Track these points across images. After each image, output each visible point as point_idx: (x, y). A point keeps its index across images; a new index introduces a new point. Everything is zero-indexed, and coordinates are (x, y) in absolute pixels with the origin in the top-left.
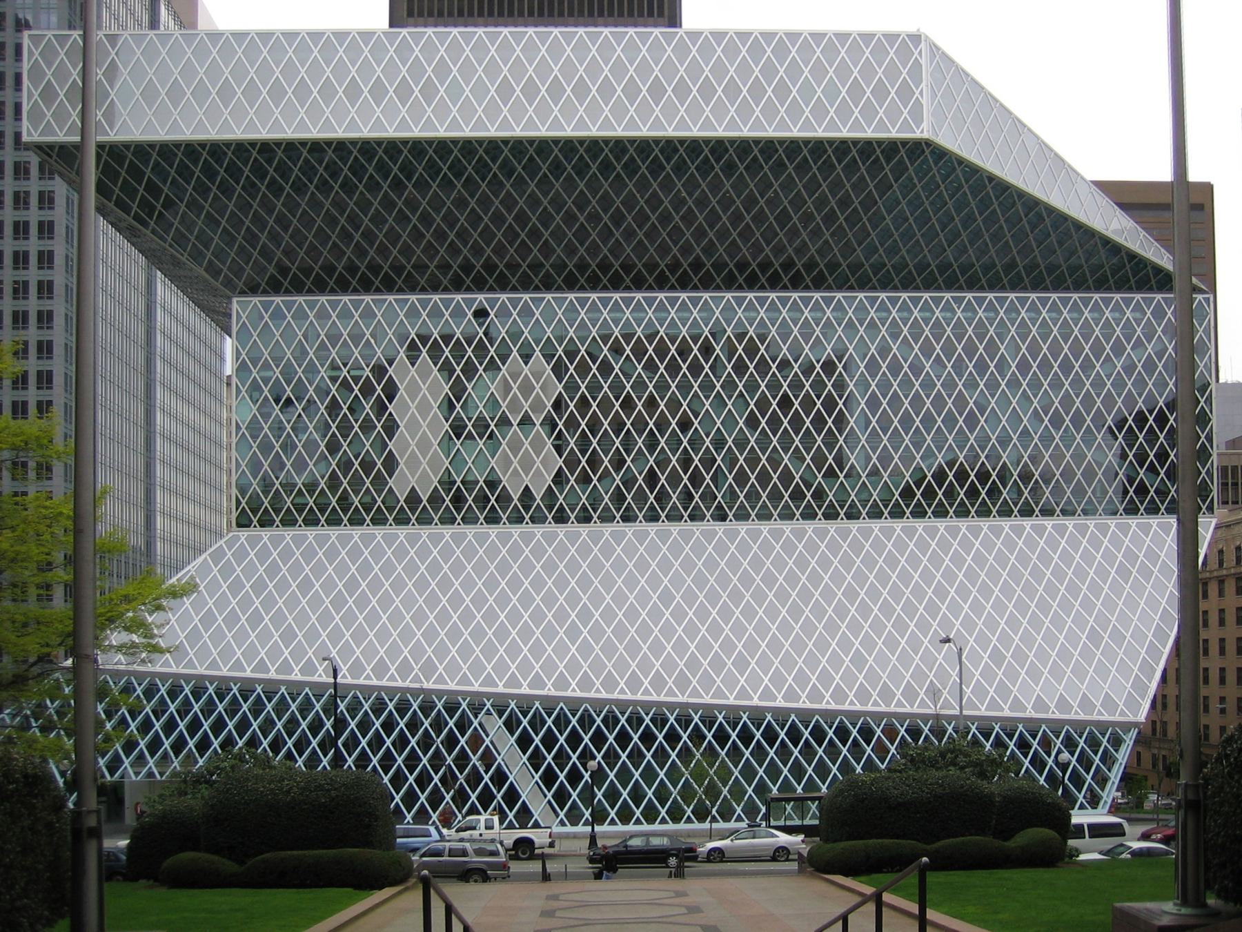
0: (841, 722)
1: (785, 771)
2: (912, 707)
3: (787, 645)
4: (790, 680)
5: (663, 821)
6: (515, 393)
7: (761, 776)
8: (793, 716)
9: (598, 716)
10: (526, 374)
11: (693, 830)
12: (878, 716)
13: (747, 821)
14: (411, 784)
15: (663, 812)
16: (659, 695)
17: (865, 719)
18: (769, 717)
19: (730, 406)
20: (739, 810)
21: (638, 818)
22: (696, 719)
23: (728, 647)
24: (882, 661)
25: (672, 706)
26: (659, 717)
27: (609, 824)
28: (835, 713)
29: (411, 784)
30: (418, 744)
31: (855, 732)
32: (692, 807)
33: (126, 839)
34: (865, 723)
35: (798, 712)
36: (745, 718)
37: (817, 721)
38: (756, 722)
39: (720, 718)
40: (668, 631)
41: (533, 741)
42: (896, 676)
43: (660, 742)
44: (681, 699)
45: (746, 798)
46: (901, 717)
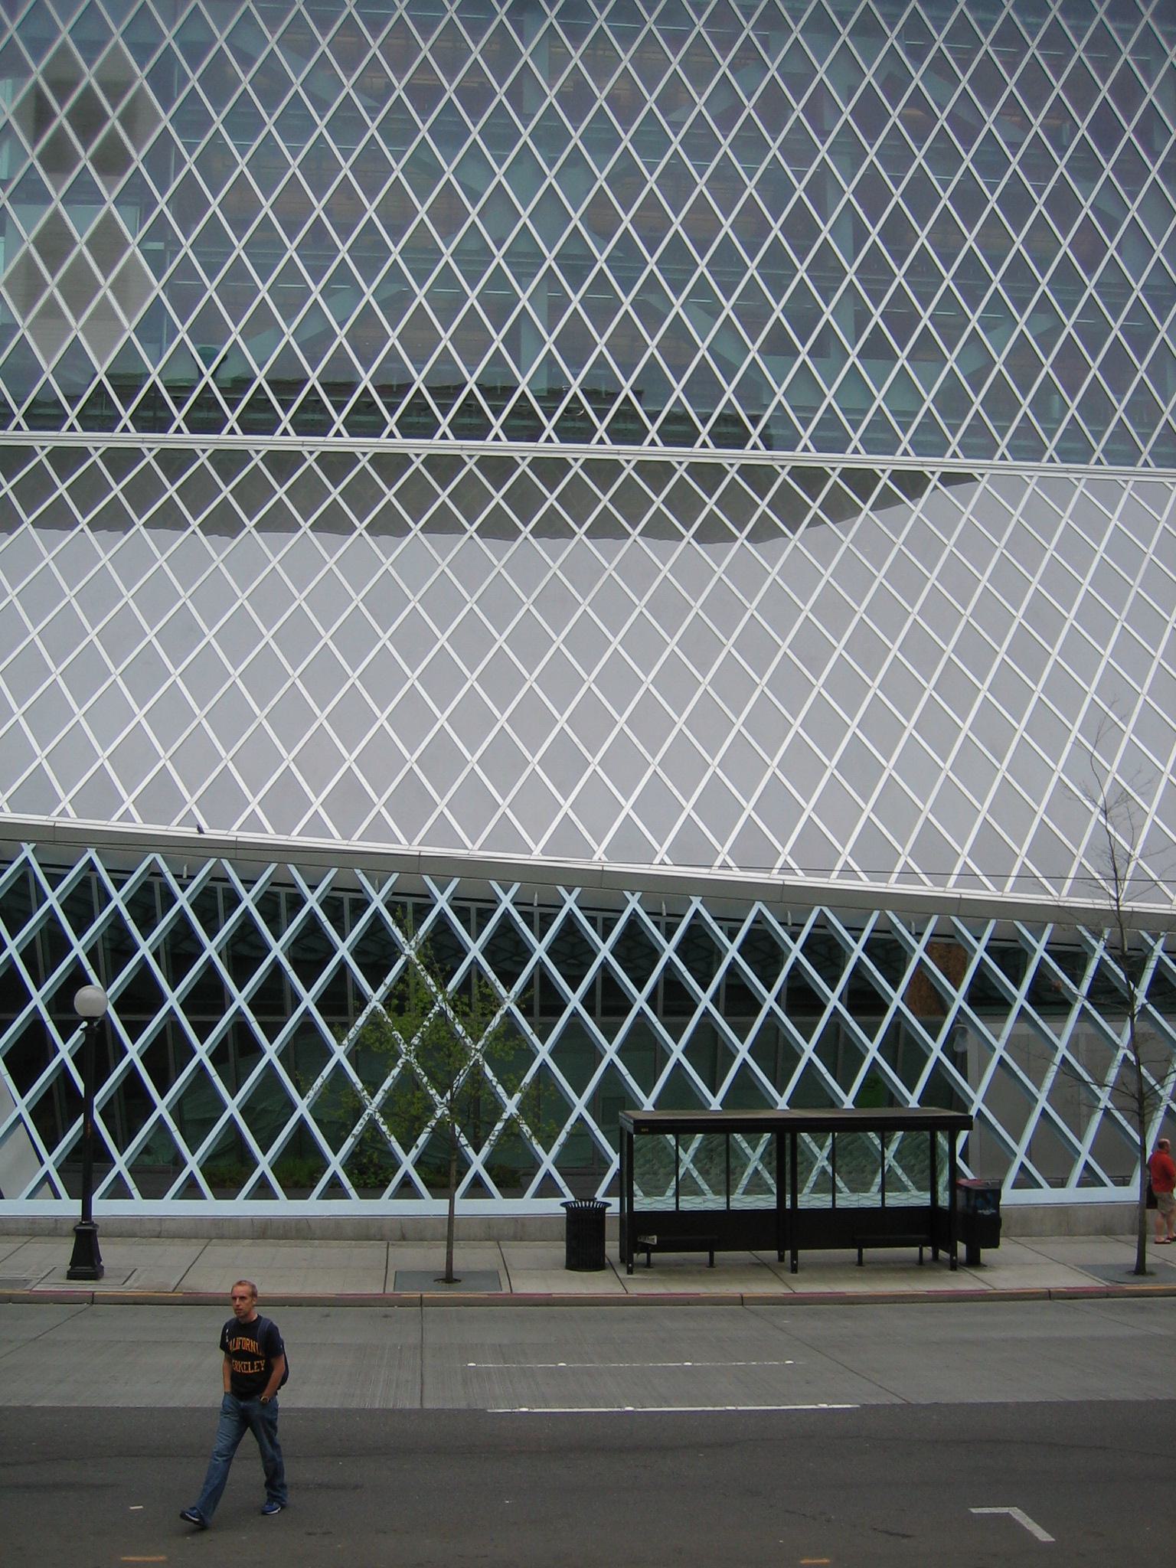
0: (822, 923)
1: (677, 1052)
2: (1001, 888)
3: (680, 723)
4: (749, 808)
5: (334, 1190)
6: (61, 128)
7: (678, 1065)
8: (696, 903)
9: (183, 888)
10: (89, 88)
11: (416, 1220)
12: (915, 908)
13: (570, 1197)
14: (270, 1065)
15: (336, 1163)
16: (347, 836)
17: (883, 917)
18: (634, 903)
19: (550, 179)
20: (547, 1162)
21: (335, 1176)
22: (442, 902)
23: (531, 719)
24: (917, 768)
25: (378, 865)
26: (347, 897)
27: (396, 1196)
28: (808, 897)
29: (270, 1065)
30: (92, 955)
31: (857, 951)
32: (486, 1150)
33: (734, 1138)
34: (885, 929)
35: (711, 890)
36: (570, 903)
37: (760, 919)
38: (600, 915)
39: (506, 902)
40: (382, 678)
41: (136, 949)
42: (953, 808)
43: (540, 963)
44: (404, 846)
45: (350, 1142)
46: (977, 912)
